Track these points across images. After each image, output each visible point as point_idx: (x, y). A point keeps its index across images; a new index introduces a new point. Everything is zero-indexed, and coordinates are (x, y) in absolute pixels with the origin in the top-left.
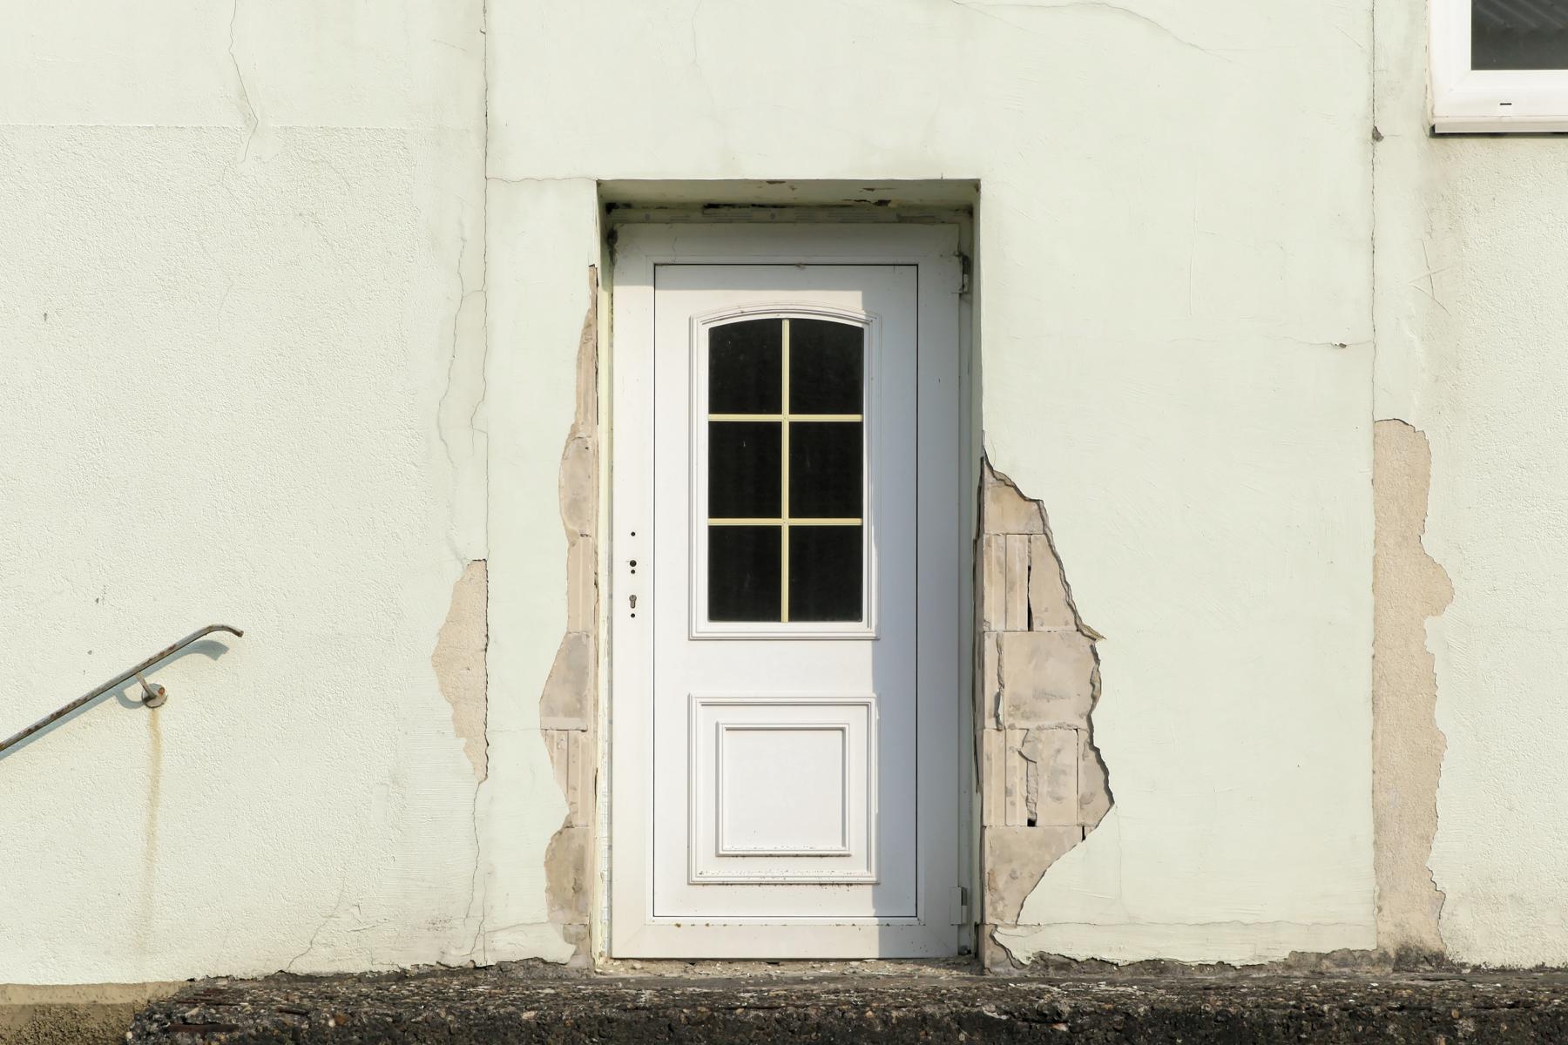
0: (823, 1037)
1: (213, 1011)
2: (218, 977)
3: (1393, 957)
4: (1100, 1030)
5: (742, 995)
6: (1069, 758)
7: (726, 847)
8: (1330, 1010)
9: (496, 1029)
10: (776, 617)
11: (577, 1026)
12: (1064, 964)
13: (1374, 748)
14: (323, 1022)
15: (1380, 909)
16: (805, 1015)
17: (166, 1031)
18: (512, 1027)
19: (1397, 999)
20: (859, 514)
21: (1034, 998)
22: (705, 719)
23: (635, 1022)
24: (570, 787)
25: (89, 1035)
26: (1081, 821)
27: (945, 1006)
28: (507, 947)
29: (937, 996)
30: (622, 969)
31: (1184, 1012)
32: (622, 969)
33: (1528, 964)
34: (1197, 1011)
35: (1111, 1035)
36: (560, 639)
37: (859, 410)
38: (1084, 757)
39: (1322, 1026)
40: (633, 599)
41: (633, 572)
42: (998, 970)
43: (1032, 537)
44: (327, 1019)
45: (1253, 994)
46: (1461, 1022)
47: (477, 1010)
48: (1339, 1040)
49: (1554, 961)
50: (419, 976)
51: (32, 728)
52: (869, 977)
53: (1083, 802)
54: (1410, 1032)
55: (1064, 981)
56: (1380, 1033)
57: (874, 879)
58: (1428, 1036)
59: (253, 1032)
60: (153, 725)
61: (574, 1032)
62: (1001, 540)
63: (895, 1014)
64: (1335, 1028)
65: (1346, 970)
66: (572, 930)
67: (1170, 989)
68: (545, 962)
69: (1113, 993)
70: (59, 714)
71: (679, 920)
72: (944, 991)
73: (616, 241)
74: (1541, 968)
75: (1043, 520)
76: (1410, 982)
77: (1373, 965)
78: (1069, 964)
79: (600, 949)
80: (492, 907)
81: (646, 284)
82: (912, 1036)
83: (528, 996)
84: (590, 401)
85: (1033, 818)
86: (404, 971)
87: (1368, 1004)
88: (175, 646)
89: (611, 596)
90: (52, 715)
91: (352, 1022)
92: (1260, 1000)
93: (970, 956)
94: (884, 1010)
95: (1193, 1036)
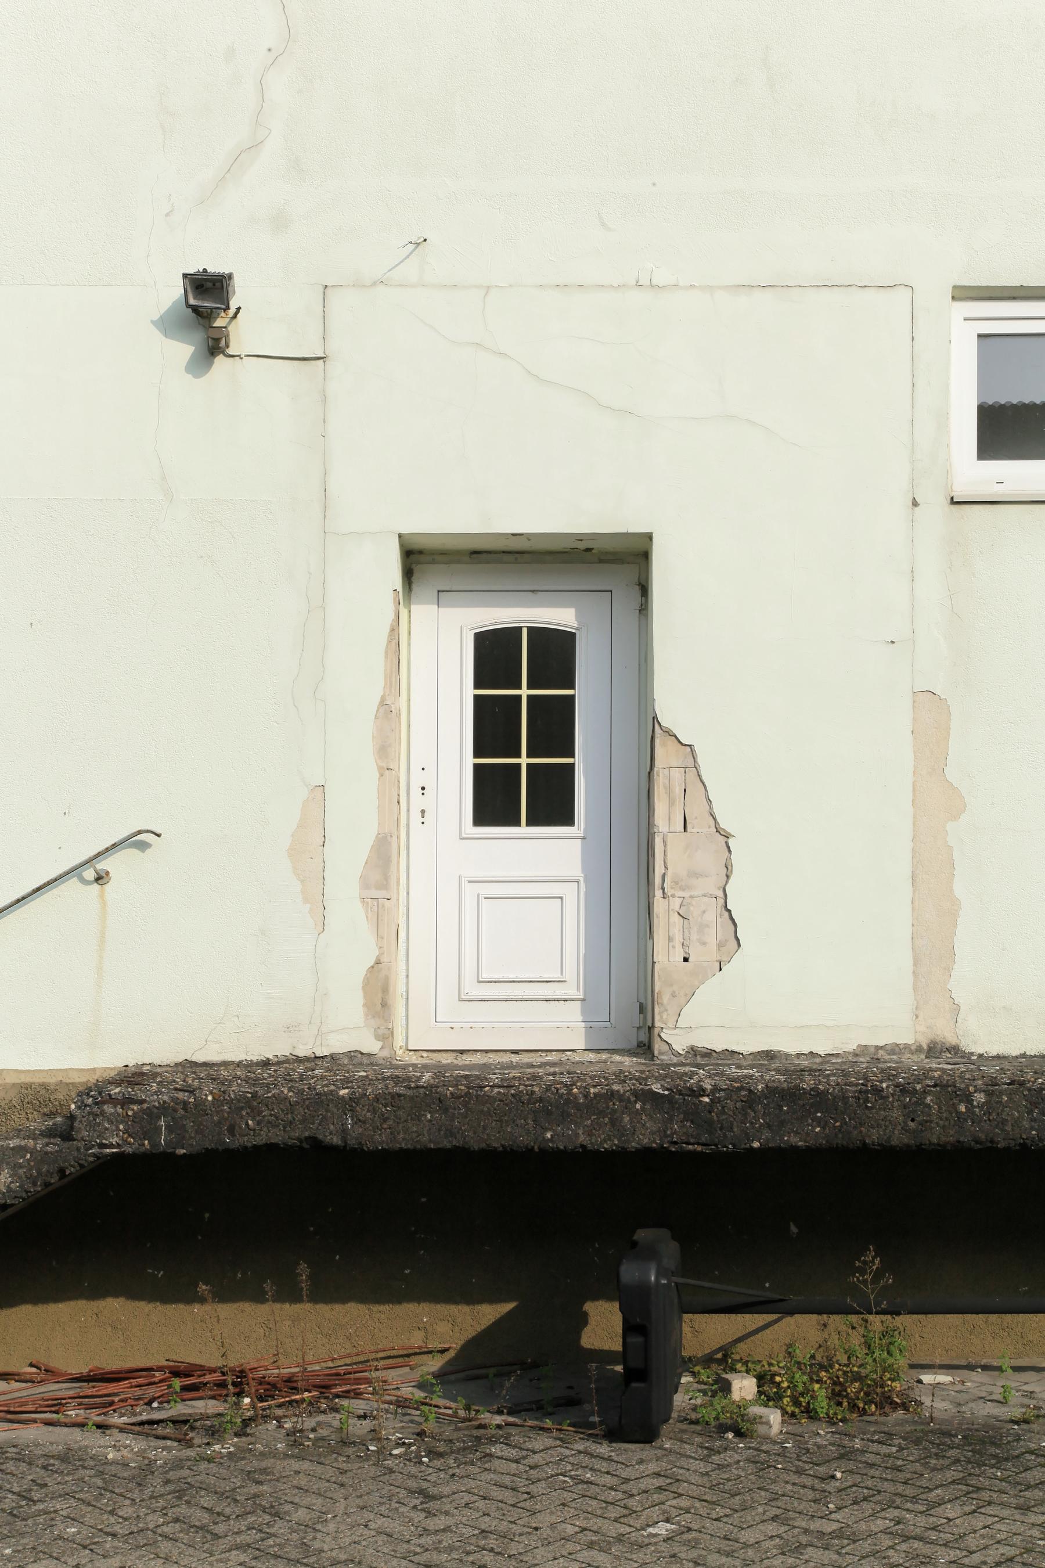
0: (544, 1106)
1: (130, 1090)
2: (143, 1064)
3: (925, 1048)
4: (731, 1101)
5: (491, 1076)
6: (711, 916)
7: (484, 976)
8: (887, 1087)
9: (322, 1102)
10: (517, 823)
11: (377, 1099)
12: (706, 1053)
13: (913, 909)
14: (204, 1097)
15: (917, 1017)
16: (532, 1091)
17: (97, 1104)
18: (333, 1100)
19: (931, 1079)
20: (573, 756)
21: (687, 1079)
22: (470, 891)
23: (417, 1097)
24: (379, 937)
25: (57, 1103)
26: (719, 958)
27: (626, 1085)
28: (336, 1044)
29: (621, 1077)
30: (415, 1057)
31: (789, 1089)
32: (415, 1057)
33: (1015, 1053)
34: (797, 1087)
35: (739, 1105)
36: (374, 838)
37: (573, 687)
38: (721, 916)
39: (882, 1098)
40: (423, 812)
41: (423, 794)
42: (663, 1057)
43: (687, 769)
44: (206, 1095)
45: (834, 1075)
46: (976, 1095)
47: (309, 1088)
48: (893, 1107)
49: (1032, 1051)
50: (278, 1063)
51: (20, 898)
52: (578, 1063)
53: (720, 946)
54: (941, 1102)
55: (707, 1065)
56: (920, 1102)
57: (582, 997)
58: (953, 1104)
59: (156, 1104)
60: (102, 896)
61: (375, 1104)
62: (666, 771)
63: (592, 1090)
64: (891, 1099)
65: (895, 1057)
66: (380, 1032)
67: (778, 1071)
68: (362, 1054)
69: (740, 1074)
70: (38, 889)
71: (452, 1025)
72: (627, 1074)
73: (412, 576)
74: (1023, 1055)
75: (694, 758)
76: (938, 1066)
77: (913, 1054)
78: (711, 1054)
79: (400, 1044)
80: (327, 1017)
81: (433, 604)
82: (604, 1106)
83: (347, 1077)
84: (394, 680)
85: (687, 956)
86: (268, 1059)
87: (912, 1083)
88: (115, 843)
89: (408, 810)
90: (34, 890)
91: (224, 1097)
92: (839, 1080)
93: (645, 1048)
94: (585, 1088)
95: (795, 1104)
